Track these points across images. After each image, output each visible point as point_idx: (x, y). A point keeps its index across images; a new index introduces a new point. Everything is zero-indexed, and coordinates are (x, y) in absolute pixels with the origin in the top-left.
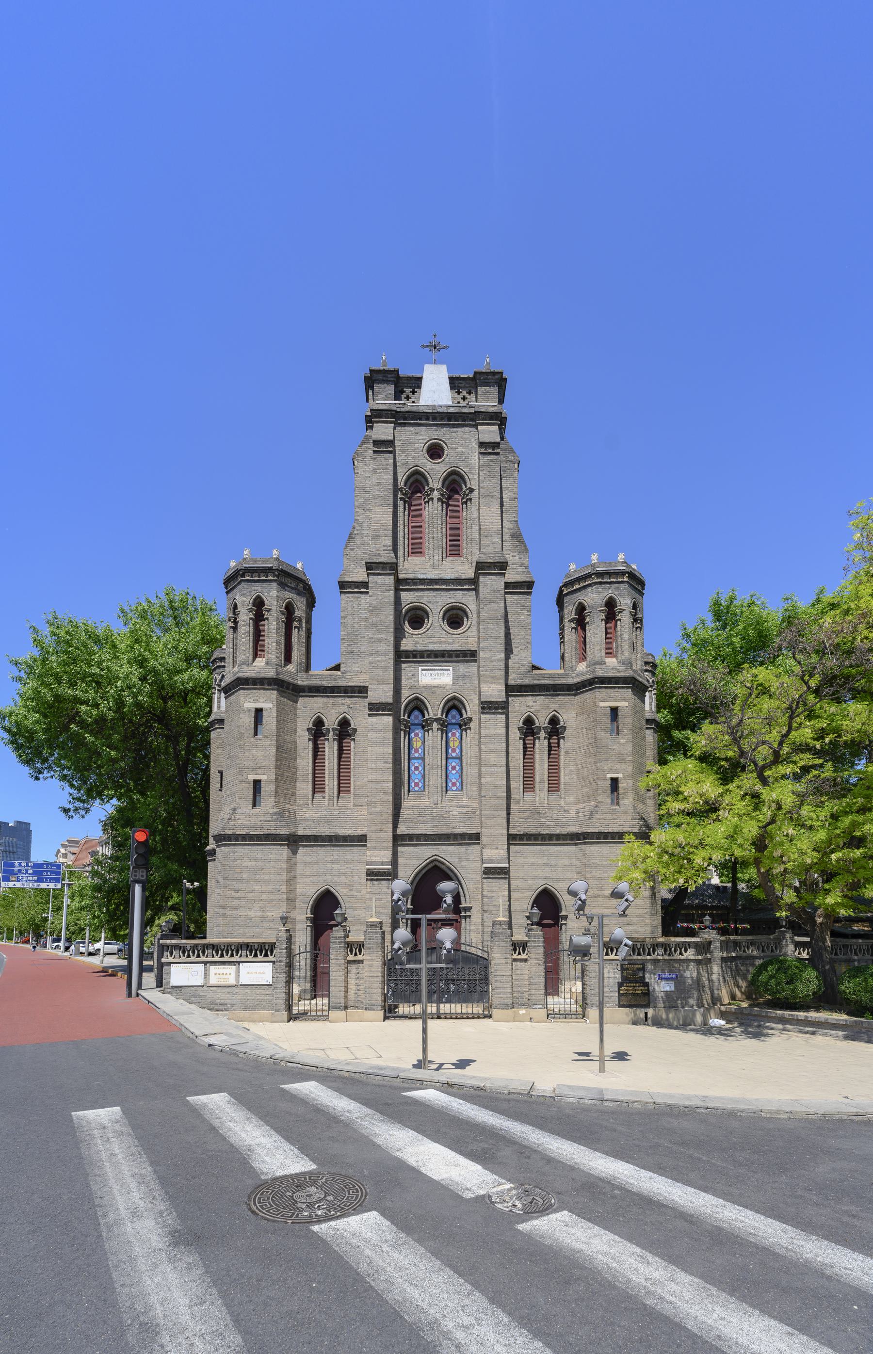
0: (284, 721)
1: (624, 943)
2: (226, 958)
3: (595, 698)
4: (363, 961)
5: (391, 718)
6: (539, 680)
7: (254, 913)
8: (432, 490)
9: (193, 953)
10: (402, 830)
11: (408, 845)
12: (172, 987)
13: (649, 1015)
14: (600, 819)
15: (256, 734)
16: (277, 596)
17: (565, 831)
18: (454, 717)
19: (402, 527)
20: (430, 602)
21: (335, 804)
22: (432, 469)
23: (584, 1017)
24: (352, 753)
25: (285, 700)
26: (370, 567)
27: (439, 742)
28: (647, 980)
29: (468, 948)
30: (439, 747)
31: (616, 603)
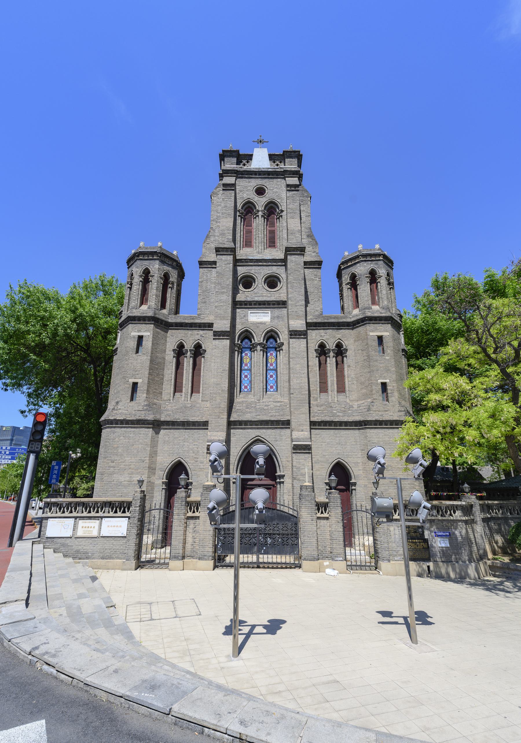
0: (158, 344)
1: (423, 505)
2: (93, 514)
3: (367, 330)
4: (199, 517)
5: (228, 341)
6: (328, 319)
7: (124, 478)
8: (258, 211)
9: (68, 509)
10: (234, 417)
11: (238, 428)
12: (47, 538)
13: (432, 568)
14: (375, 411)
15: (137, 352)
16: (159, 268)
17: (351, 419)
18: (271, 343)
19: (239, 231)
20: (256, 273)
21: (189, 399)
22: (258, 200)
23: (376, 568)
24: (202, 366)
25: (158, 330)
26: (219, 250)
27: (261, 359)
28: (426, 537)
29: (282, 507)
30: (261, 362)
31: (376, 272)
